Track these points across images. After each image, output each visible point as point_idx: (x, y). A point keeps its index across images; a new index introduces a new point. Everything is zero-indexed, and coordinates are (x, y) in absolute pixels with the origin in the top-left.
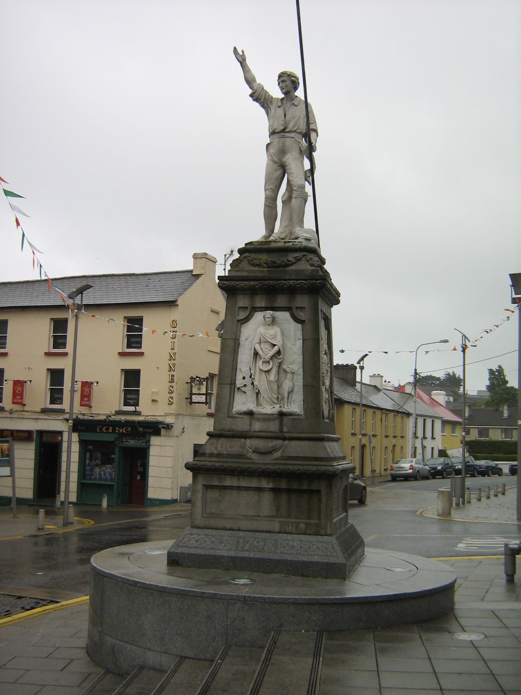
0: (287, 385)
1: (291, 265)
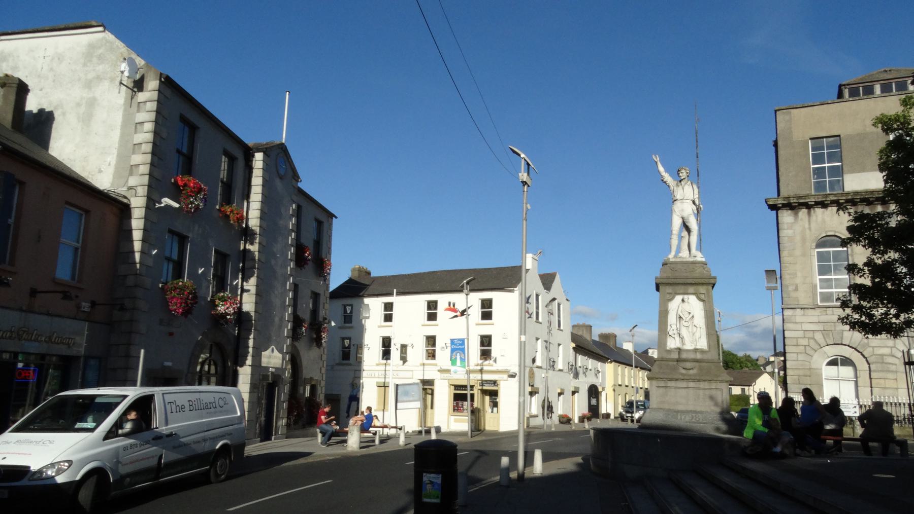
0: (697, 335)
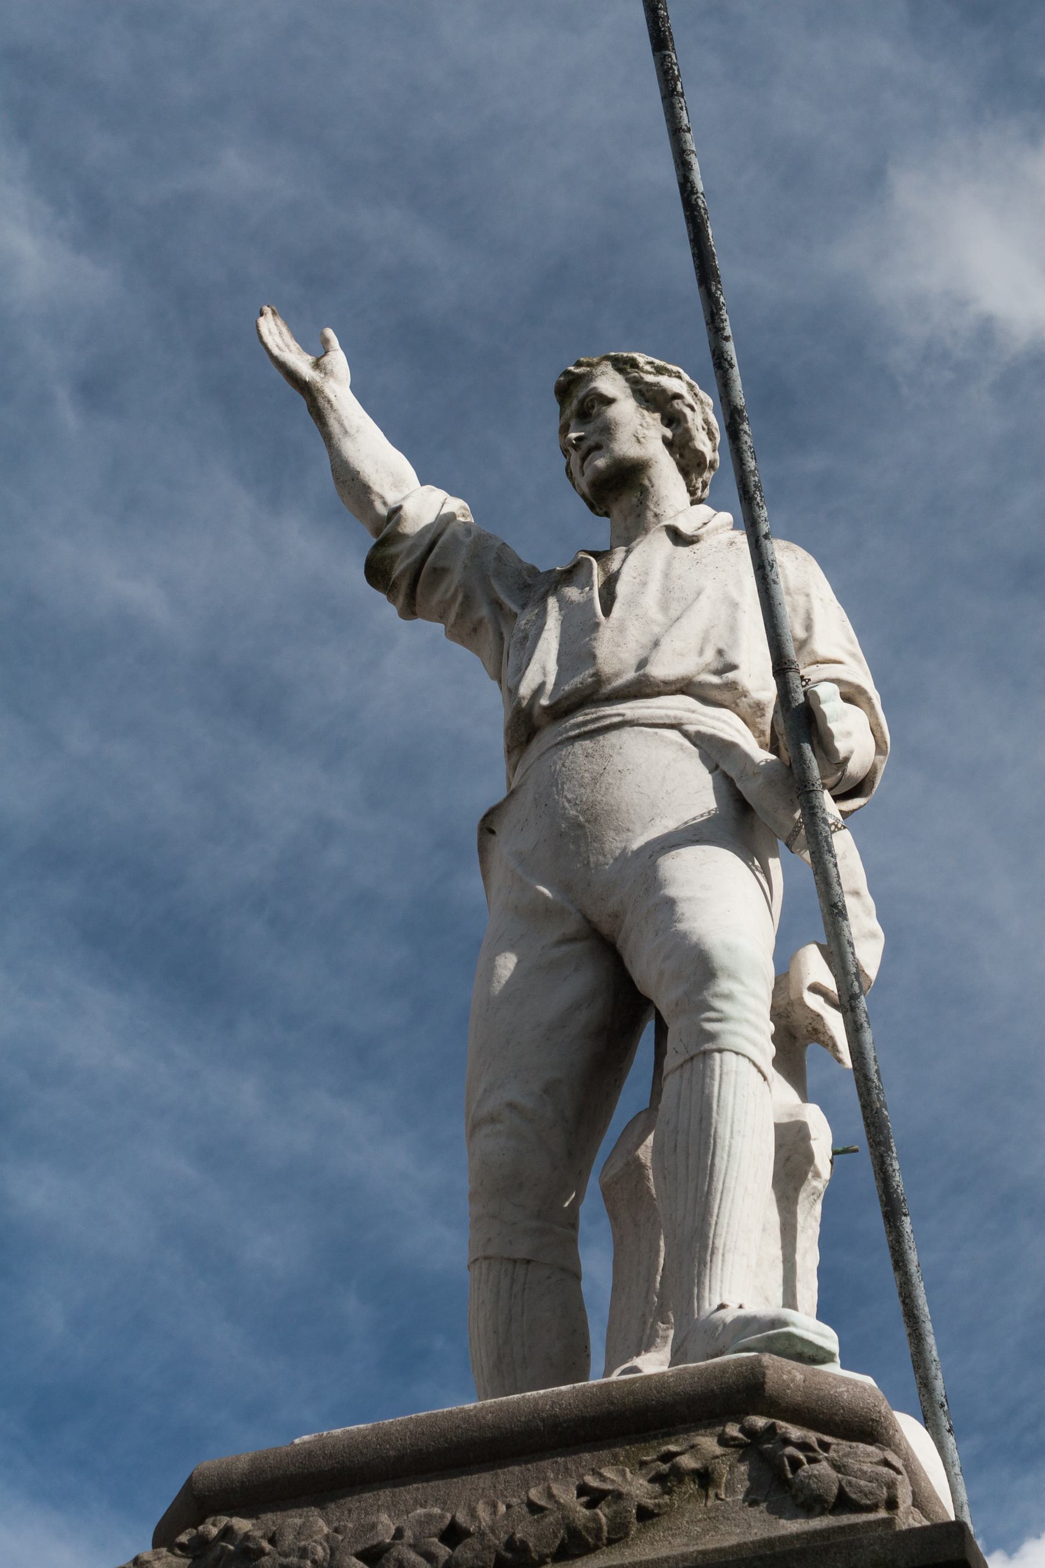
1: (618, 1535)
